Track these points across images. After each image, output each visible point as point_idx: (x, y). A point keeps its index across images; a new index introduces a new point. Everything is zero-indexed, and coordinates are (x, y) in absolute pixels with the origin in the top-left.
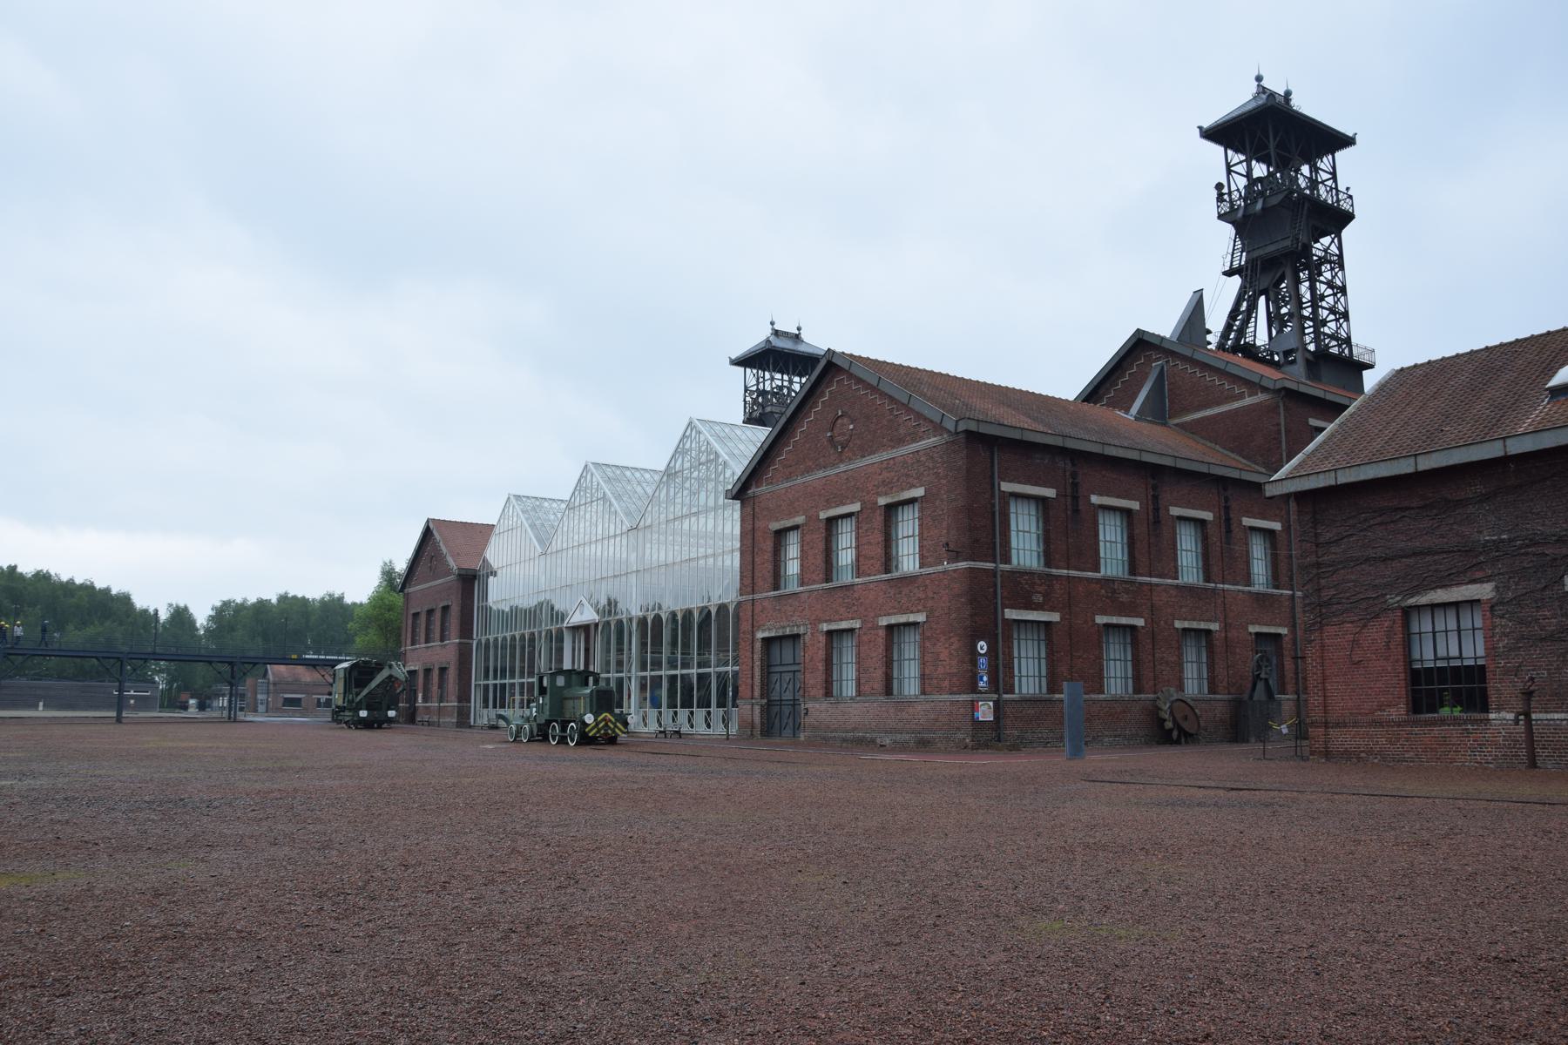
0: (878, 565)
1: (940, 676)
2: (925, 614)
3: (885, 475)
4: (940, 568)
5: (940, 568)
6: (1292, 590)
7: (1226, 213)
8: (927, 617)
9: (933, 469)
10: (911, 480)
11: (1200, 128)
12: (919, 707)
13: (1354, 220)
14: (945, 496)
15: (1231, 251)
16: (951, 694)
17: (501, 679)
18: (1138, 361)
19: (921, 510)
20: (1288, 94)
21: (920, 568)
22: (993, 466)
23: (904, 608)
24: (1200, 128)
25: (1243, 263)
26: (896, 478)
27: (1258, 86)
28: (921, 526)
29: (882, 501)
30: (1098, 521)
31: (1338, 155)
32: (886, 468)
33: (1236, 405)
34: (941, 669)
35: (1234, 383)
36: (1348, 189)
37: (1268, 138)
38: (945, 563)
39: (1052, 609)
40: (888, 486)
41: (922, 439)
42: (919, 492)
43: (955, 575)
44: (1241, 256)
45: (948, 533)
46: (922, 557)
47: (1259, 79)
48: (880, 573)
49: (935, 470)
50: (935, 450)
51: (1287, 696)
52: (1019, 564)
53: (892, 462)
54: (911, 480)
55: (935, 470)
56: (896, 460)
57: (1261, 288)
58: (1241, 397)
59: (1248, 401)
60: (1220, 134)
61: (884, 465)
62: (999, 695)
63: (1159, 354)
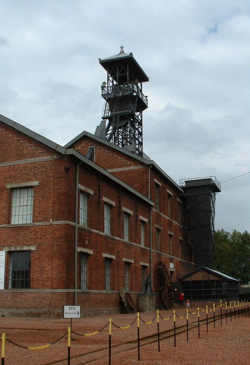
0: (4, 219)
1: (44, 279)
2: (35, 247)
3: (11, 173)
4: (47, 223)
5: (47, 223)
6: (150, 248)
7: (105, 95)
8: (37, 248)
9: (45, 172)
10: (29, 177)
11: (100, 59)
12: (29, 295)
13: (147, 108)
14: (52, 186)
15: (104, 110)
16: (51, 289)
17: (18, 279)
18: (81, 144)
19: (35, 192)
20: (131, 54)
21: (33, 222)
22: (76, 175)
23: (20, 242)
24: (100, 59)
25: (109, 115)
26: (19, 175)
27: (121, 50)
28: (34, 200)
29: (9, 186)
30: (104, 210)
31: (143, 83)
32: (13, 169)
33: (127, 169)
34: (45, 276)
35: (127, 159)
36: (147, 96)
37: (116, 71)
38: (51, 221)
39: (91, 249)
40: (13, 178)
41: (38, 156)
42: (36, 183)
43: (57, 227)
44: (109, 112)
45: (53, 205)
46: (34, 216)
47: (122, 48)
48: (5, 223)
49: (46, 173)
50: (47, 163)
51: (133, 292)
52: (81, 225)
53: (17, 166)
54: (29, 177)
55: (46, 173)
56: (19, 165)
57: (119, 126)
58: (130, 165)
59: (133, 168)
60: (108, 64)
61: (12, 168)
62: (75, 290)
63: (92, 143)
